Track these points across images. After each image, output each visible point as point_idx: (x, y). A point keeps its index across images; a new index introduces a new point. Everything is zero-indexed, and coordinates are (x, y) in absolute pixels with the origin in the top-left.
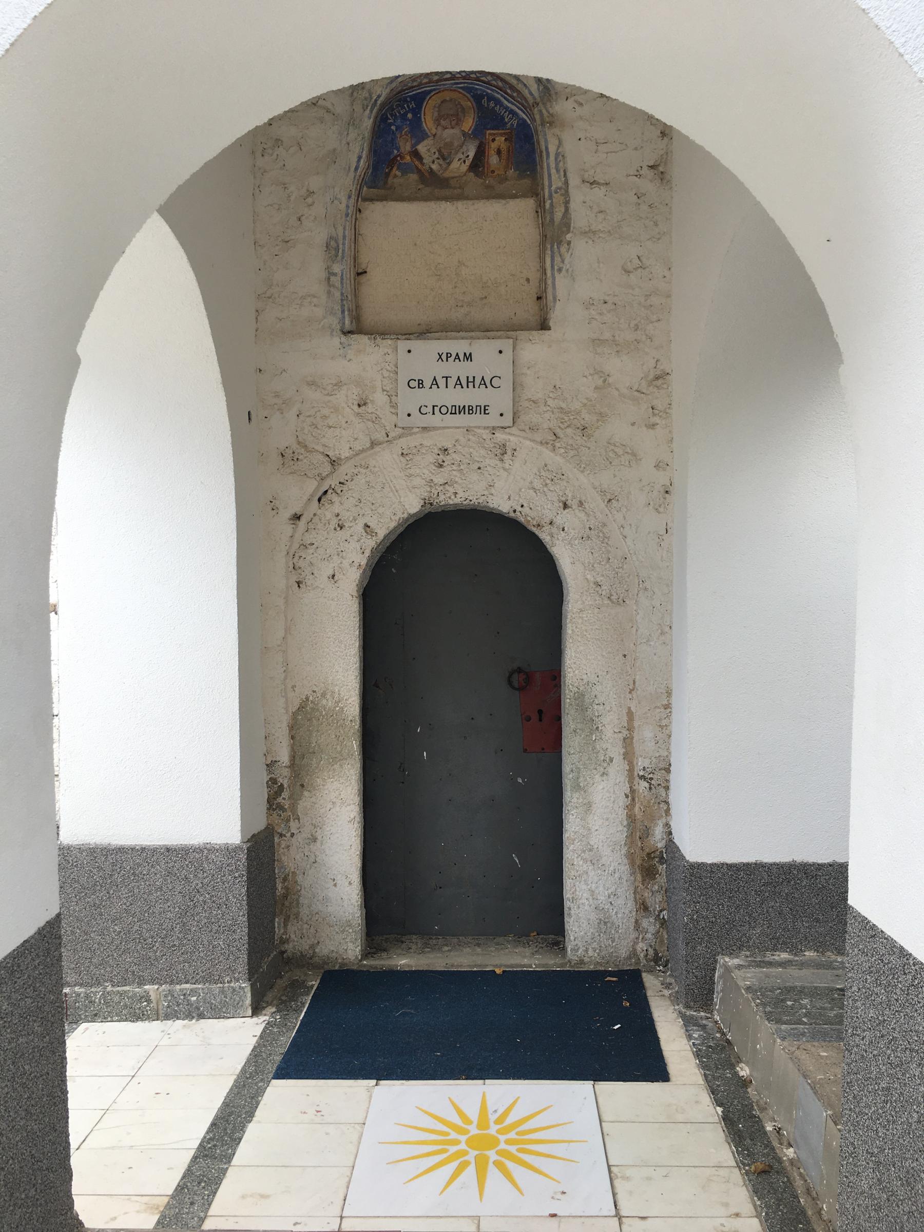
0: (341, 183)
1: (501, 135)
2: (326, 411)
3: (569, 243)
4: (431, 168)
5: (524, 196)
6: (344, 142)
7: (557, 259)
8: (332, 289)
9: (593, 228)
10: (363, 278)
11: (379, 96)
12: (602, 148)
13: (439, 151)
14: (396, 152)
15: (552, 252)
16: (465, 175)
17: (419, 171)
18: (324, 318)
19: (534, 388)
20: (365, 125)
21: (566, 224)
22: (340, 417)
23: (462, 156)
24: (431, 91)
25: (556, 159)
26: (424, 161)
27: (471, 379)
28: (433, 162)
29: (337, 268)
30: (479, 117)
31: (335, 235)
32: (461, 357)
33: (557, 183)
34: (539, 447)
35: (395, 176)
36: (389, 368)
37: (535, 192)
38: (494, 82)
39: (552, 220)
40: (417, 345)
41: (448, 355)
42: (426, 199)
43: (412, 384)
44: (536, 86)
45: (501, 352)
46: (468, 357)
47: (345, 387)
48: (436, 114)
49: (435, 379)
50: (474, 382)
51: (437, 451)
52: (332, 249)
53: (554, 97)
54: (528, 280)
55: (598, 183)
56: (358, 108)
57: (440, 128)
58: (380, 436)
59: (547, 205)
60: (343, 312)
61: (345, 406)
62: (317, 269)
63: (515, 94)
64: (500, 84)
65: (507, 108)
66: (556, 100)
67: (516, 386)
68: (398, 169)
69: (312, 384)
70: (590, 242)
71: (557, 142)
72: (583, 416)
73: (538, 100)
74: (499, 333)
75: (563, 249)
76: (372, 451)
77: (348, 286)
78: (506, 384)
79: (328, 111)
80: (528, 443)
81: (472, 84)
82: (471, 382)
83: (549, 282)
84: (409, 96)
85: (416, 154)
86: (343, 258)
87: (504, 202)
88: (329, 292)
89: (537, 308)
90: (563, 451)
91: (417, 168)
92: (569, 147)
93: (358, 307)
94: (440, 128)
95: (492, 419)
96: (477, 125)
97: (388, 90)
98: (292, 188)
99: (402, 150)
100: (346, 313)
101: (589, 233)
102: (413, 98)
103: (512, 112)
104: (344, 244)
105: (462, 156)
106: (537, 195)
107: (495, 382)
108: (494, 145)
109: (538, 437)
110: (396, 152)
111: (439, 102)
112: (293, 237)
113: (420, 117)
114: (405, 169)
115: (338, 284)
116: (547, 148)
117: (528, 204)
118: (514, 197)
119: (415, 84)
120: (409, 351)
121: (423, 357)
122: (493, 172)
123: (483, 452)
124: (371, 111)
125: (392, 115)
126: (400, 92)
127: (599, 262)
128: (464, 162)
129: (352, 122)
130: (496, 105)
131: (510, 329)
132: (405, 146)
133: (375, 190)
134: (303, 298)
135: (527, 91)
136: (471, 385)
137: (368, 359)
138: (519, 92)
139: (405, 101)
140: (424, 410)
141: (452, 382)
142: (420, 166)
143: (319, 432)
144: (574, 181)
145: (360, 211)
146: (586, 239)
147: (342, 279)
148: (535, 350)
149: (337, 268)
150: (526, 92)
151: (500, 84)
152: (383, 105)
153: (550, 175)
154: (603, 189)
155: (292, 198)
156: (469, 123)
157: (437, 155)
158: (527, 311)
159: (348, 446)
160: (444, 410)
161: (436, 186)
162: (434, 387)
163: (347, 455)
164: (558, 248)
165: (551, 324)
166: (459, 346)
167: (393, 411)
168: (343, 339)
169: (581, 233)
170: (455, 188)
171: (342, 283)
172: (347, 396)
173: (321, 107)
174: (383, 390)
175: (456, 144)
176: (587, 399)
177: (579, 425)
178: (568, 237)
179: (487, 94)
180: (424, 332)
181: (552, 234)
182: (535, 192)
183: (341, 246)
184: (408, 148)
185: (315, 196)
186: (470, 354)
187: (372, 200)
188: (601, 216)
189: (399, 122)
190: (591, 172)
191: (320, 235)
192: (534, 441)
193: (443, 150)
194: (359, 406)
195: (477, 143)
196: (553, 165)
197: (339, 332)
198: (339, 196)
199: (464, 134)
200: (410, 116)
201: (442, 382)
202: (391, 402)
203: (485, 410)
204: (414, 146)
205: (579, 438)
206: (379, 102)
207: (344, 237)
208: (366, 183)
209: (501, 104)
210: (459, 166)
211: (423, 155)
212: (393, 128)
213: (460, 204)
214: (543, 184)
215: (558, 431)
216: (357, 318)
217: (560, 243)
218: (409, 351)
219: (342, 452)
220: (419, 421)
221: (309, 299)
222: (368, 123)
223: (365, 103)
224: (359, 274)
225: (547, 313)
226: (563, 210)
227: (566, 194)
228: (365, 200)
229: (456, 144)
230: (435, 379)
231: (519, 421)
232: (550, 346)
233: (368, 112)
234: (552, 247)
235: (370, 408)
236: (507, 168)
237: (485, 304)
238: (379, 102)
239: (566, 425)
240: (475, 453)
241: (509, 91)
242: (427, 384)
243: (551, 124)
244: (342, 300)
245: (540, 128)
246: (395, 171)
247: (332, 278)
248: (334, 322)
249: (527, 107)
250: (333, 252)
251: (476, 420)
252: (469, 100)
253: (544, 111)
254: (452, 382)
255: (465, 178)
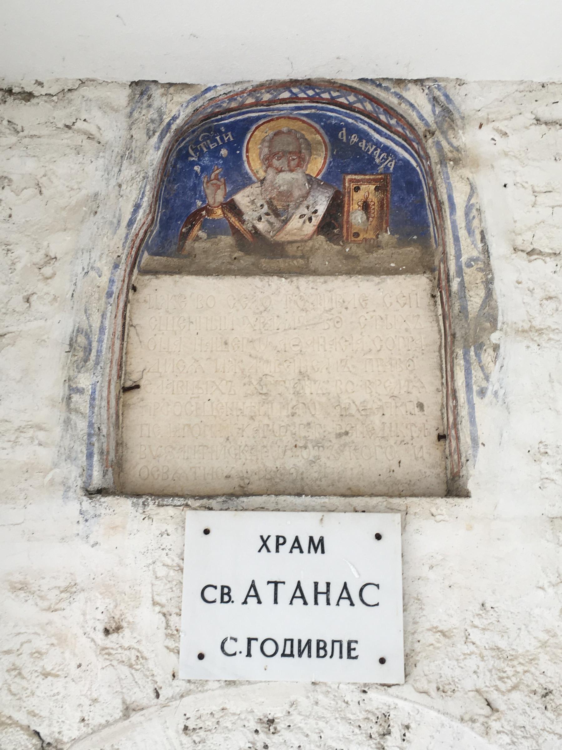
0: (107, 244)
1: (369, 182)
2: (41, 643)
3: (496, 348)
4: (254, 227)
5: (411, 271)
6: (113, 182)
7: (477, 374)
8: (73, 417)
9: (537, 323)
10: (133, 397)
11: (174, 118)
12: (542, 198)
13: (270, 203)
14: (199, 203)
15: (467, 361)
16: (311, 238)
17: (236, 232)
18: (56, 465)
19: (442, 609)
20: (148, 158)
21: (490, 316)
22: (67, 655)
23: (305, 211)
24: (258, 118)
25: (467, 214)
26: (246, 217)
27: (322, 588)
28: (260, 219)
29: (85, 381)
30: (333, 156)
31: (85, 326)
32: (305, 544)
33: (470, 250)
34: (456, 724)
35: (198, 238)
36: (169, 562)
37: (429, 263)
38: (359, 105)
39: (464, 310)
40: (220, 520)
41: (280, 541)
42: (246, 273)
43: (211, 594)
44: (429, 107)
45: (378, 537)
46: (318, 545)
47: (81, 597)
48: (266, 150)
49: (253, 586)
50: (327, 592)
51: (253, 725)
52: (80, 348)
53: (459, 122)
54: (421, 406)
55: (540, 253)
56: (139, 134)
57: (271, 172)
58: (142, 694)
59: (455, 285)
60: (90, 456)
61: (80, 632)
62: (50, 381)
63: (393, 122)
64: (369, 107)
65: (378, 144)
66: (463, 128)
67: (408, 601)
68: (202, 228)
69: (20, 588)
70: (534, 347)
71: (468, 189)
72: (543, 668)
73: (434, 127)
74: (375, 501)
75: (487, 357)
76: (127, 722)
77: (104, 412)
78: (390, 598)
79: (90, 137)
80: (433, 714)
81: (322, 109)
82: (321, 592)
83: (464, 412)
84: (225, 125)
85: (232, 207)
86: (97, 363)
87: (376, 279)
88: (67, 422)
89: (439, 453)
90: (506, 739)
91: (232, 226)
92: (487, 195)
93: (120, 444)
94: (271, 172)
95: (364, 669)
96: (330, 167)
97: (190, 110)
98: (19, 251)
99: (210, 200)
100: (96, 458)
101: (531, 332)
102: (230, 127)
103: (386, 149)
104: (100, 341)
105: (305, 211)
106: (432, 270)
107: (370, 594)
108: (358, 197)
109: (454, 706)
110: (199, 203)
111: (271, 133)
112: (10, 329)
113: (240, 155)
114: (214, 229)
115: (85, 407)
116: (450, 198)
117: (418, 285)
118: (395, 272)
119: (233, 105)
120: (207, 532)
121: (231, 543)
122: (357, 235)
123: (344, 729)
124: (161, 139)
125: (195, 150)
126: (208, 118)
127: (551, 381)
128: (310, 219)
129: (128, 154)
130: (360, 140)
131: (394, 491)
132: (216, 196)
133: (163, 259)
134: (20, 430)
135: (414, 115)
136: (322, 598)
137: (133, 535)
138: (400, 117)
139: (217, 130)
140: (230, 647)
141: (286, 592)
142: (237, 224)
143: (24, 683)
144: (499, 248)
145: (134, 289)
146: (526, 343)
147: (93, 399)
148: (438, 527)
149: (85, 381)
150: (413, 117)
151: (369, 107)
152: (180, 134)
153: (457, 239)
154: (551, 263)
155: (19, 266)
156: (317, 165)
157: (266, 209)
158: (420, 459)
159: (78, 716)
160: (269, 648)
161: (262, 254)
162: (252, 601)
163: (75, 734)
164: (478, 355)
165: (471, 486)
166: (299, 524)
167: (171, 644)
168: (87, 504)
169: (517, 332)
170: (294, 257)
171: (92, 406)
172: (84, 614)
173: (78, 131)
174: (155, 603)
175: (297, 193)
176: (548, 631)
177: (535, 686)
178: (495, 337)
179: (347, 125)
180: (235, 494)
181: (462, 332)
182: (429, 263)
183: (95, 345)
184: (220, 197)
185: (57, 264)
186: (321, 540)
187: (155, 272)
188: (550, 305)
189: (206, 160)
190: (528, 236)
191: (60, 325)
192: (445, 714)
193: (275, 203)
194: (107, 632)
195: (330, 193)
196: (461, 222)
197: (80, 492)
198: (98, 265)
199: (310, 180)
200: (224, 152)
201: (266, 592)
202: (168, 626)
203: (349, 650)
204: (228, 195)
205: (536, 713)
206: (174, 127)
207: (102, 329)
208: (148, 248)
209: (369, 139)
210: (300, 226)
211: (243, 208)
212: (197, 168)
213: (303, 282)
214: (444, 253)
215: (494, 696)
216: (117, 464)
217: (480, 347)
218: (207, 532)
219: (65, 728)
220: (218, 666)
221: (31, 433)
222: (154, 156)
223: (152, 126)
224: (126, 390)
225: (460, 465)
226: (482, 293)
227: (487, 268)
228: (144, 272)
229: (297, 193)
230: (253, 586)
231: (416, 672)
232: (470, 528)
233: (155, 139)
234: (466, 354)
235: (125, 638)
236: (379, 229)
237: (345, 445)
238: (174, 127)
239: (510, 684)
240: (327, 733)
241: (383, 118)
242: (239, 593)
243: (457, 161)
244: (90, 435)
245: (437, 168)
246: (197, 231)
247: (76, 397)
248: (72, 473)
249: (412, 137)
250: (81, 354)
251: (332, 668)
252: (318, 132)
253: (444, 143)
254: (286, 592)
255: (310, 243)
